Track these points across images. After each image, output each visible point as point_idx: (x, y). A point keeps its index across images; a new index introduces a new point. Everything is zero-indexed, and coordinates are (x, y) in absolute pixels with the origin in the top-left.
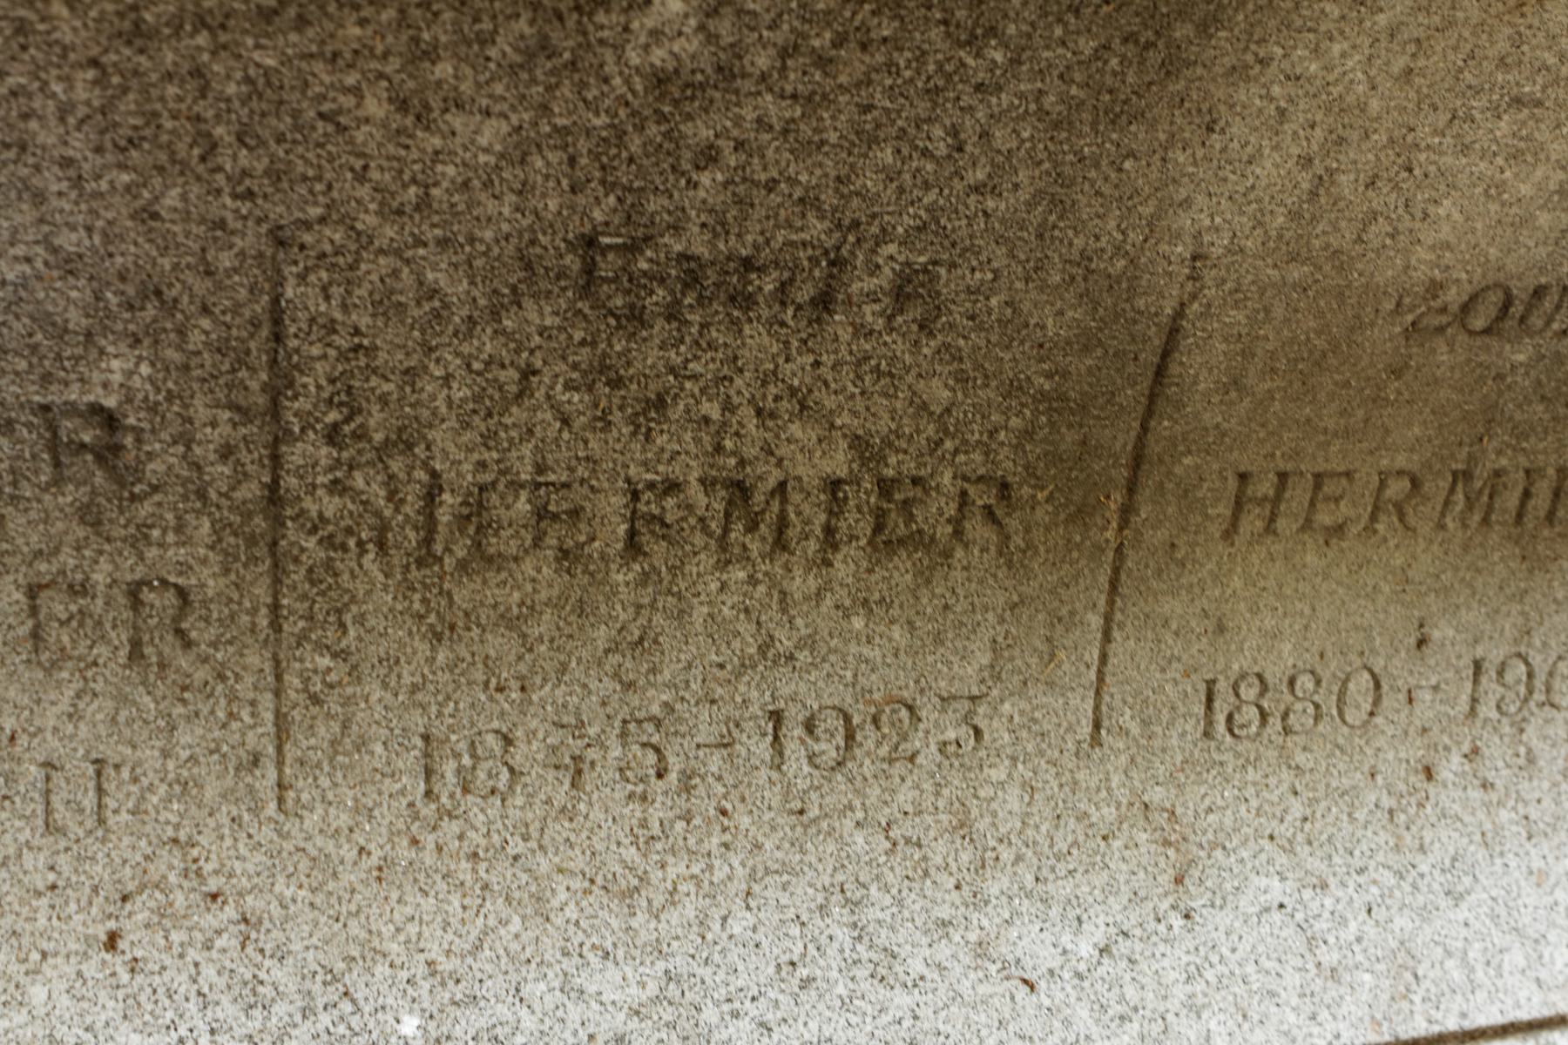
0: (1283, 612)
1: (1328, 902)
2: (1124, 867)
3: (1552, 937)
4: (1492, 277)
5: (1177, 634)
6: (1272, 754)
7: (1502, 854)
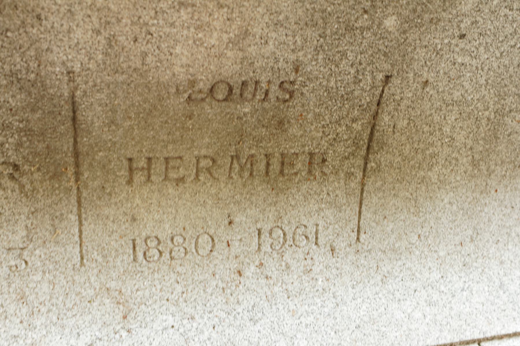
0: (163, 212)
1: (195, 325)
2: (99, 313)
3: (299, 336)
4: (217, 78)
5: (113, 221)
6: (165, 268)
7: (276, 304)
